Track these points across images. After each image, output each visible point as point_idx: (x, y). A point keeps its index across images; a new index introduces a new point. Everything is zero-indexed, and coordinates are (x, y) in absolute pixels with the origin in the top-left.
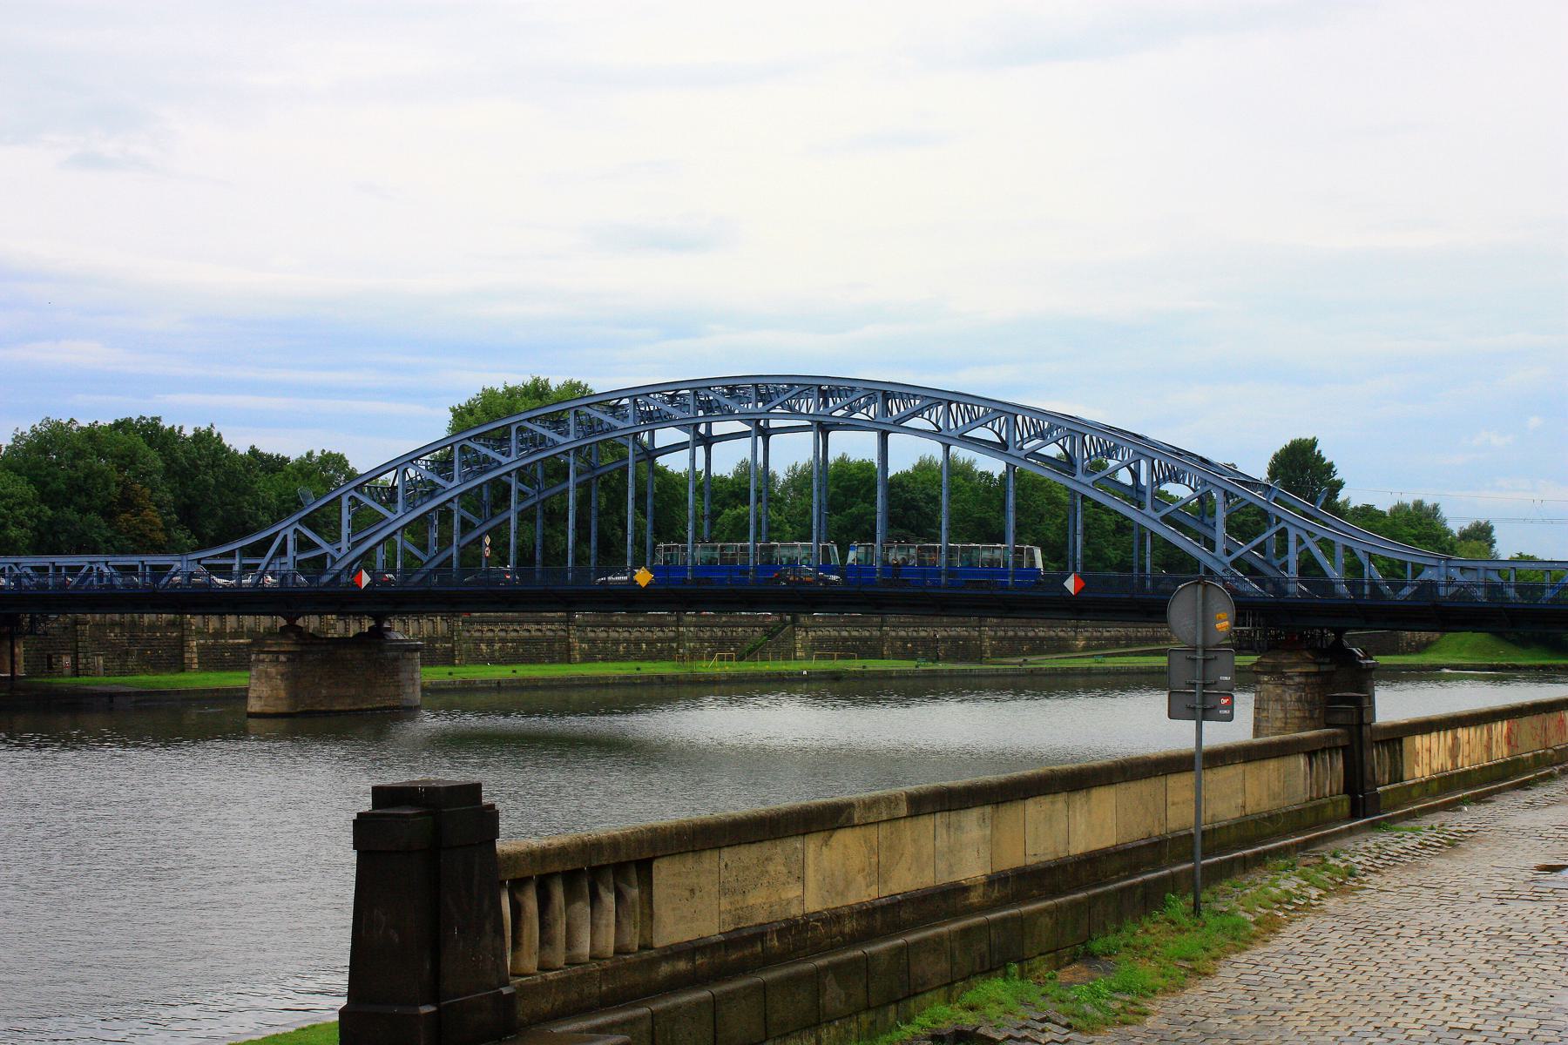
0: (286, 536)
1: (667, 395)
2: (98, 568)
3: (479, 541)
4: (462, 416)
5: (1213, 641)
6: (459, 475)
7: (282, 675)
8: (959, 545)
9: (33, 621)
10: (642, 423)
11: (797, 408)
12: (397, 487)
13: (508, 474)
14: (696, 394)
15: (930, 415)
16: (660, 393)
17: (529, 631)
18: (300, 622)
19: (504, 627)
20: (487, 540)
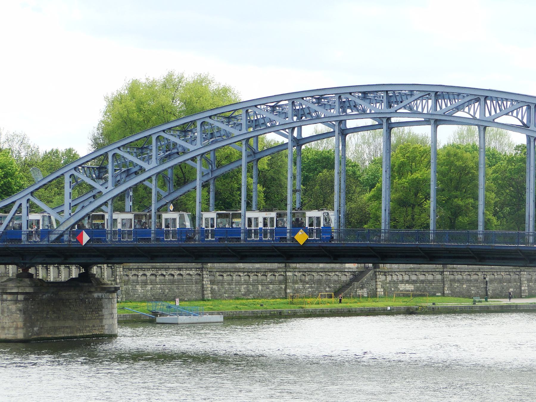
0: (21, 205)
1: (270, 106)
6: (156, 159)
7: (20, 311)
8: (231, 213)
11: (415, 108)
13: (193, 159)
14: (340, 97)
15: (517, 114)
17: (173, 275)
18: (32, 271)
19: (154, 272)
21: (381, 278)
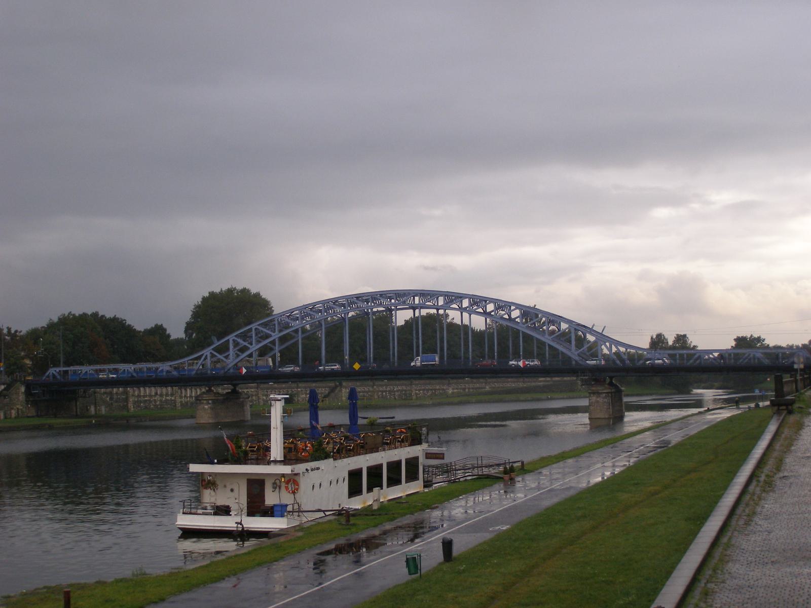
2: (128, 370)
4: (84, 313)
7: (210, 408)
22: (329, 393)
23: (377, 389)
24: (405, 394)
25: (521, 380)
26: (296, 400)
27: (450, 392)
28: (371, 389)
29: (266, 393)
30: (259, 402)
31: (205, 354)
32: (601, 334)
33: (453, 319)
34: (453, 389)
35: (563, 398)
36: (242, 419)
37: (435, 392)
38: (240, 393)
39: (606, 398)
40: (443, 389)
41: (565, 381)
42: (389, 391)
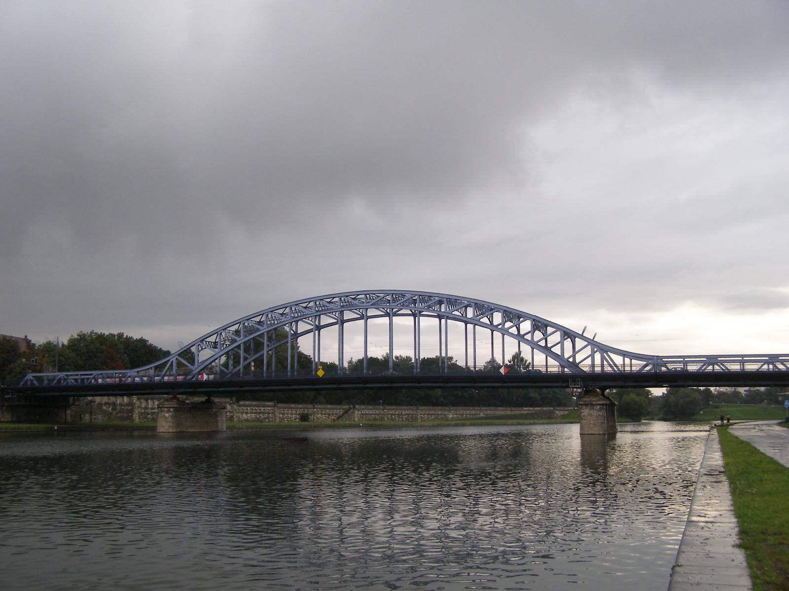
3: (249, 364)
5: (593, 415)
7: (171, 417)
9: (74, 400)
10: (388, 304)
12: (217, 342)
16: (374, 294)
17: (244, 409)
20: (253, 364)
21: (356, 412)
22: (343, 414)
23: (388, 413)
24: (412, 418)
25: (509, 409)
26: (312, 419)
27: (451, 417)
28: (382, 412)
29: (283, 412)
30: (275, 419)
31: (171, 361)
32: (593, 340)
33: (457, 361)
34: (453, 415)
35: (543, 424)
36: (214, 429)
37: (438, 416)
38: (214, 403)
39: (601, 411)
40: (445, 415)
41: (544, 410)
42: (398, 414)
